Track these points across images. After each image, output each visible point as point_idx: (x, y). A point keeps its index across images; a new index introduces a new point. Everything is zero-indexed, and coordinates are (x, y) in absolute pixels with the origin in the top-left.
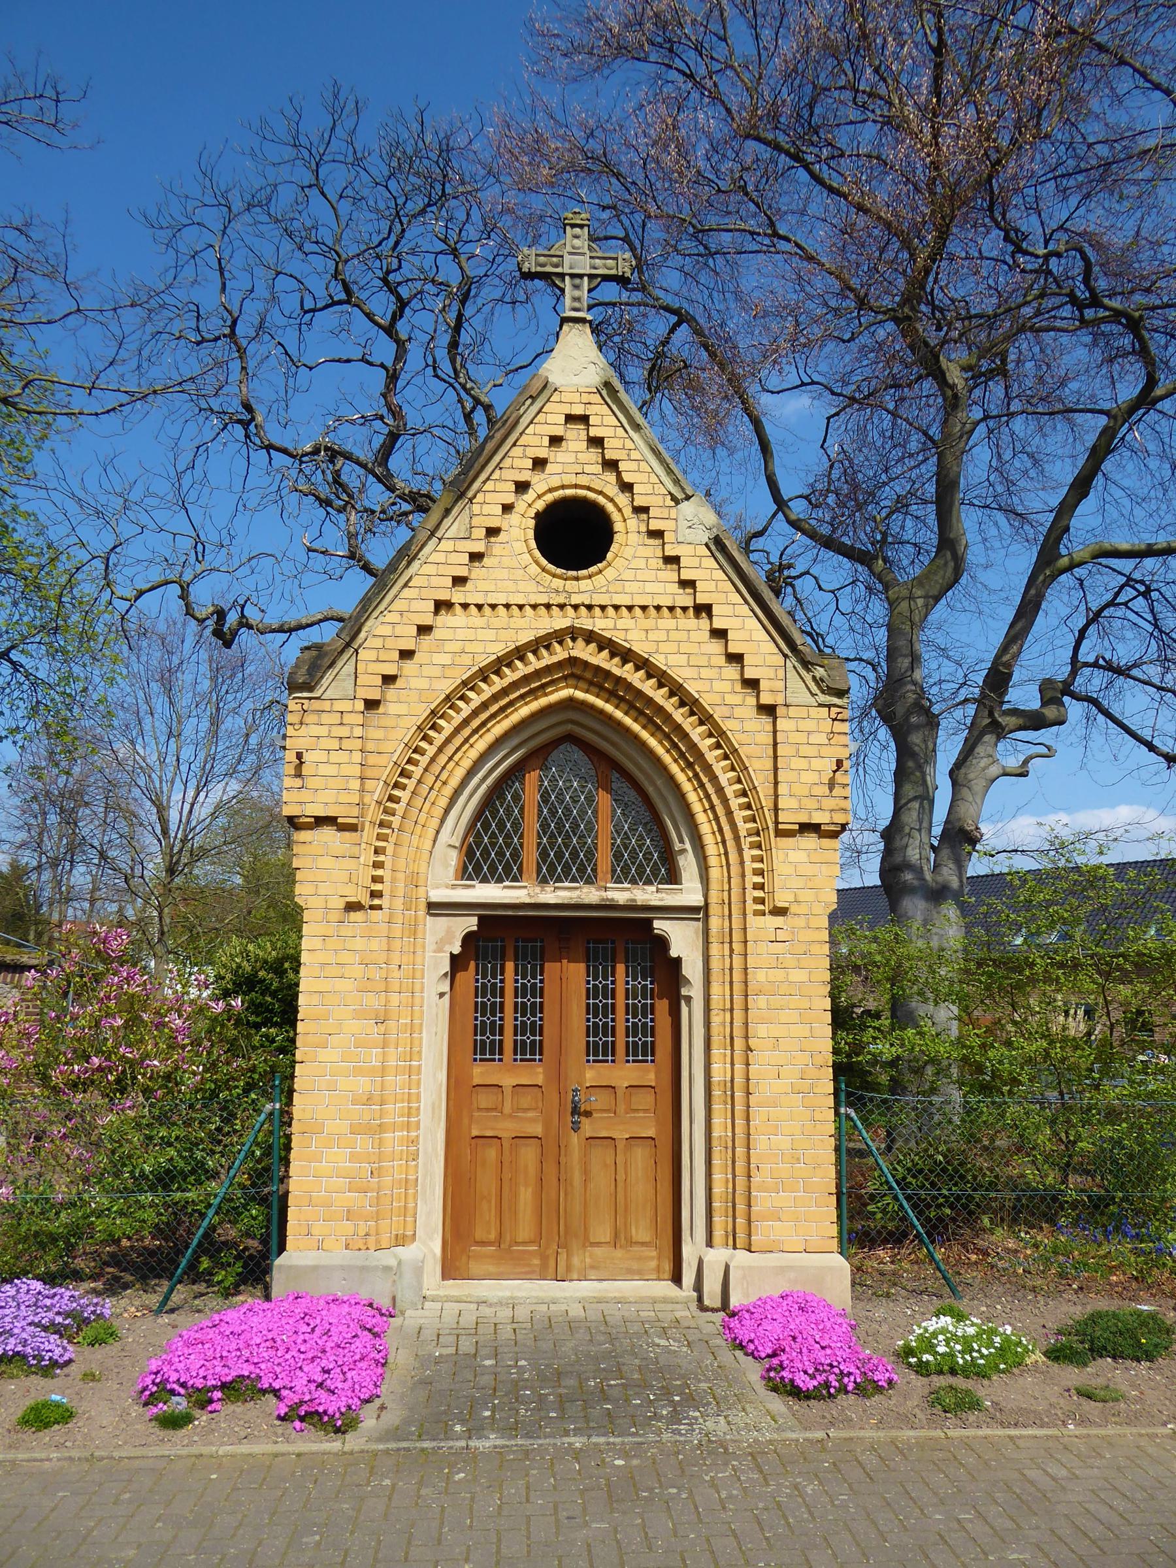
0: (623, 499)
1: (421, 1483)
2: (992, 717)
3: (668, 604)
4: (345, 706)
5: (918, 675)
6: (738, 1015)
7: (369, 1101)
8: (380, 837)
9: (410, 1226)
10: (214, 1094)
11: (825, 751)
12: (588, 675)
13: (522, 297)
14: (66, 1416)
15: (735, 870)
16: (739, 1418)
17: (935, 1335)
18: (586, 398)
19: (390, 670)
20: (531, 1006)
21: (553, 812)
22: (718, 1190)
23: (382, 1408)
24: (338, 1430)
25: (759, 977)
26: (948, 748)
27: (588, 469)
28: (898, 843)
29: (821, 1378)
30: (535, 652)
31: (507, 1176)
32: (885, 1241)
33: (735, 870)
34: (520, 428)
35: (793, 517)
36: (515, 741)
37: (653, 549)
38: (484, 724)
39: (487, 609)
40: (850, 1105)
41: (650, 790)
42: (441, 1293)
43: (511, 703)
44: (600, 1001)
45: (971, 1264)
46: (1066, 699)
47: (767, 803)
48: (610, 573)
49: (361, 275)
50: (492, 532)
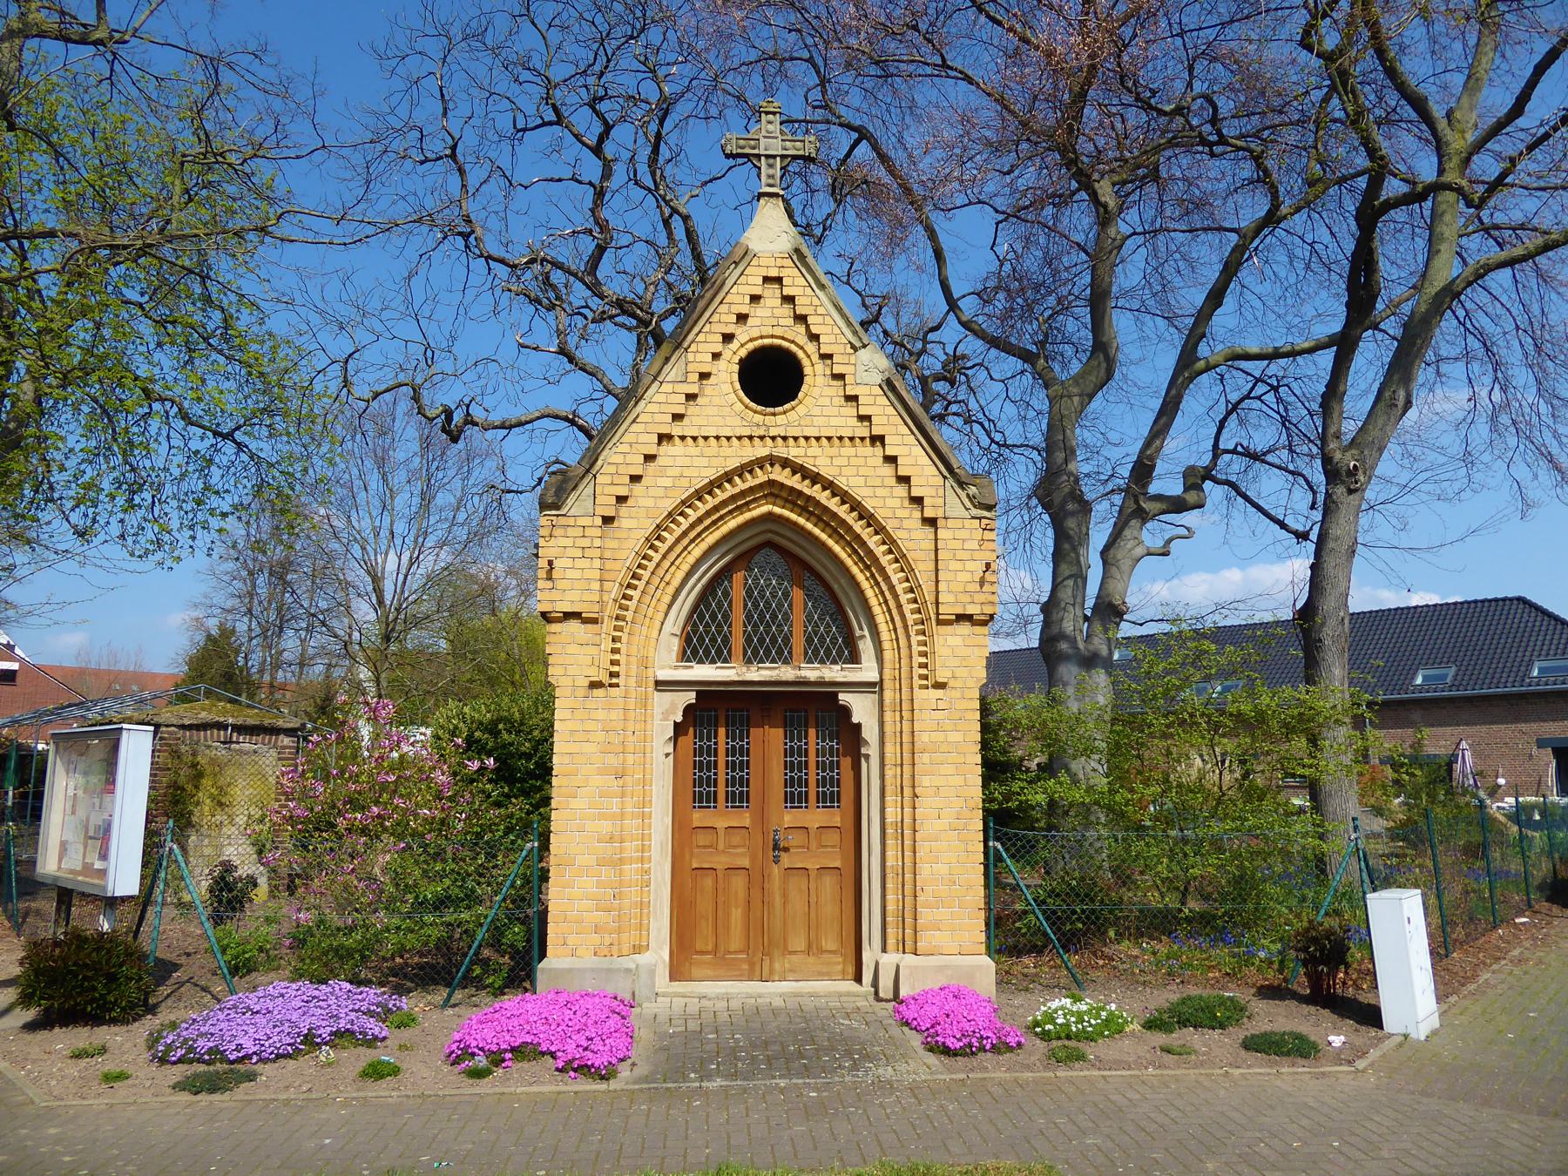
0: (811, 347)
1: (669, 1108)
2: (1138, 500)
3: (849, 431)
4: (586, 521)
5: (1072, 467)
6: (907, 768)
7: (611, 839)
8: (616, 628)
9: (644, 938)
10: (479, 836)
11: (977, 555)
12: (784, 494)
13: (714, 112)
14: (395, 1071)
15: (904, 652)
16: (903, 1067)
17: (1056, 1011)
18: (780, 262)
19: (623, 492)
20: (740, 763)
21: (756, 606)
22: (890, 907)
23: (634, 1064)
24: (603, 1078)
25: (923, 738)
26: (1099, 536)
27: (782, 322)
28: (1055, 617)
29: (965, 1041)
30: (740, 476)
31: (721, 899)
32: (1029, 952)
33: (904, 652)
34: (726, 289)
35: (964, 319)
36: (724, 548)
37: (836, 389)
38: (699, 535)
39: (701, 440)
40: (997, 839)
41: (836, 587)
42: (670, 990)
43: (721, 518)
44: (796, 759)
45: (1096, 967)
46: (1208, 485)
47: (930, 598)
48: (801, 409)
49: (571, 99)
50: (704, 376)
